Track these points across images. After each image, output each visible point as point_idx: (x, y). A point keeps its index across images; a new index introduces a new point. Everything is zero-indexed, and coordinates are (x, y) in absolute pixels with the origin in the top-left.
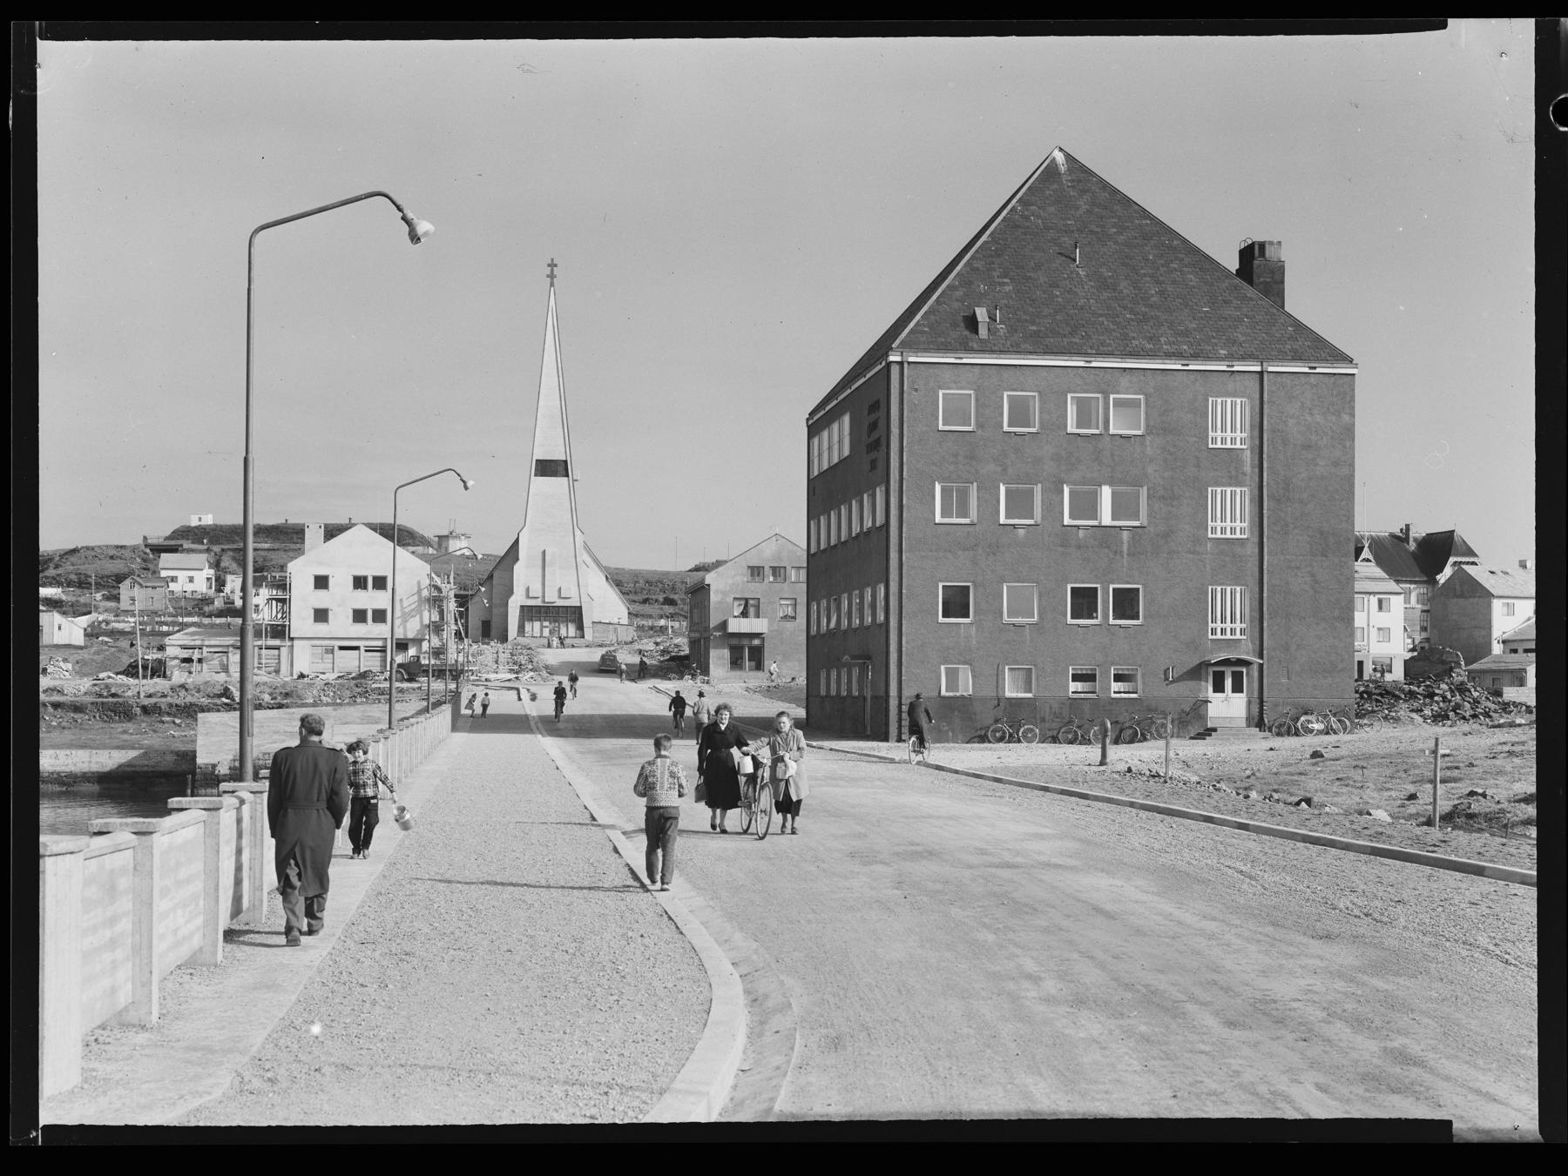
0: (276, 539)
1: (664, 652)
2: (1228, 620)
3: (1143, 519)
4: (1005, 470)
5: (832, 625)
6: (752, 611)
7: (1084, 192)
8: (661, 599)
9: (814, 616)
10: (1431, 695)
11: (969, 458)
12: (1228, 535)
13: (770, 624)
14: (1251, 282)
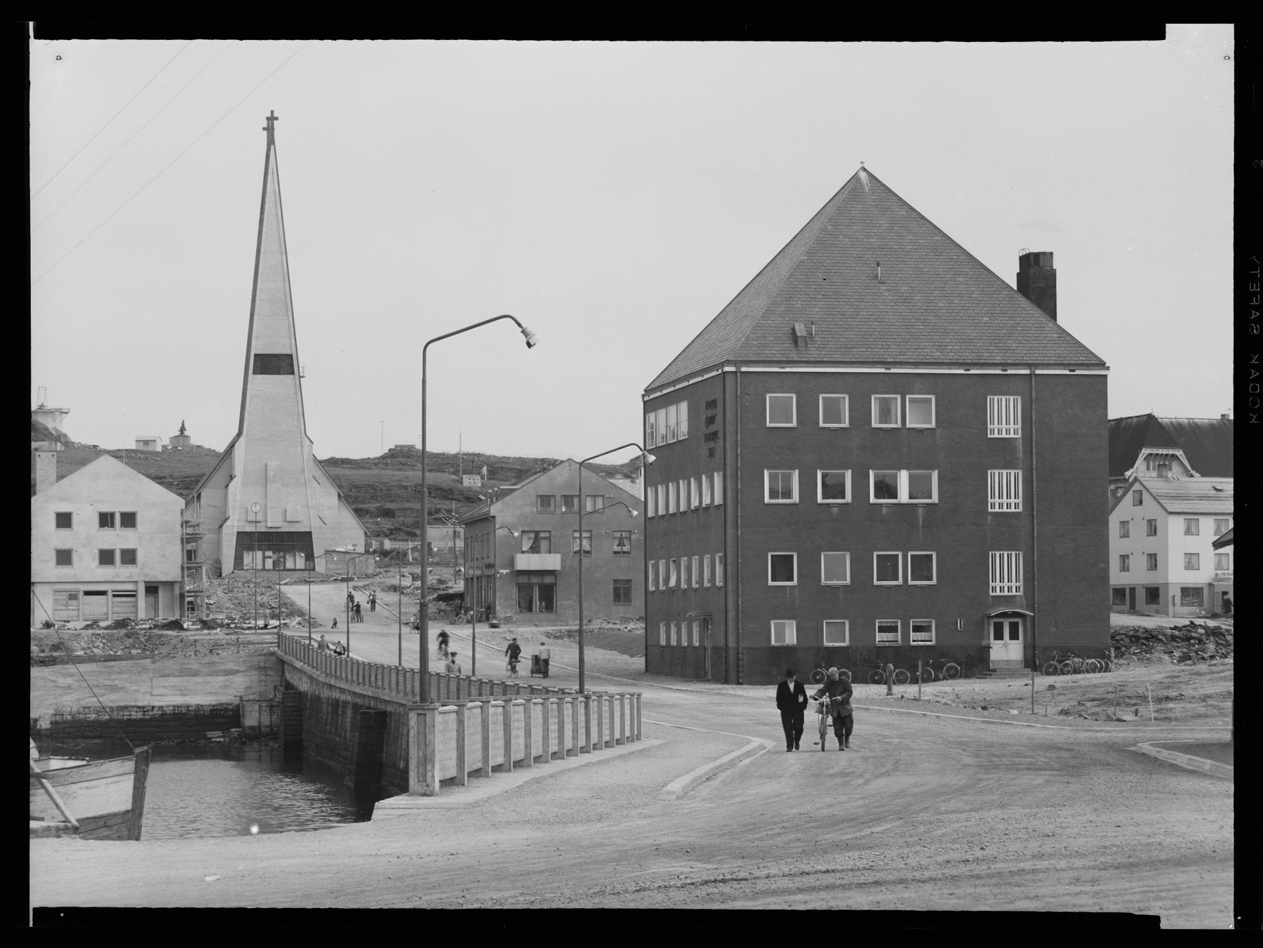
5: (672, 583)
6: (544, 545)
12: (1005, 510)
13: (563, 561)
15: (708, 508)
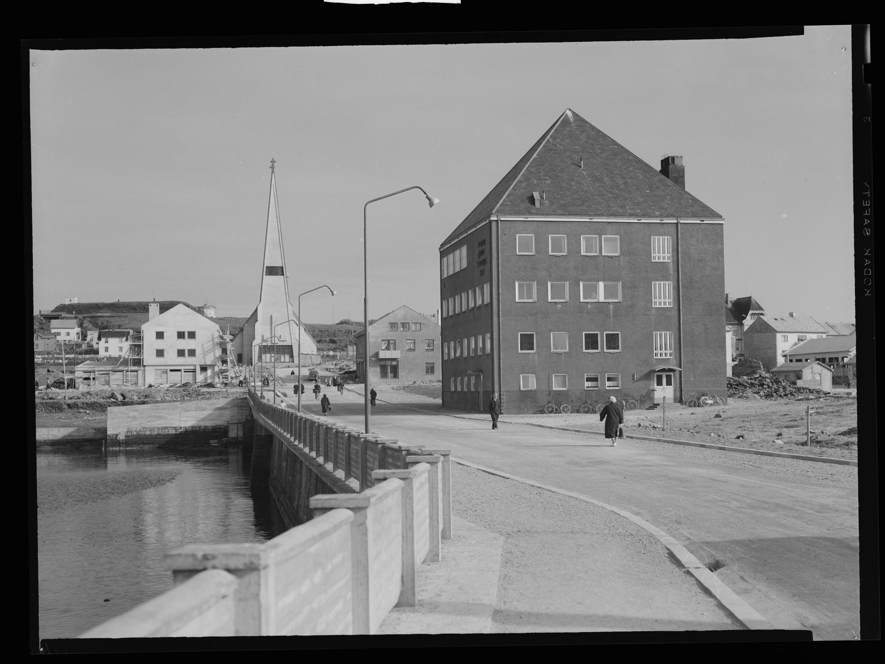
0: (113, 311)
1: (341, 369)
3: (620, 299)
4: (550, 274)
5: (458, 354)
6: (392, 346)
7: (583, 131)
8: (328, 340)
9: (446, 351)
10: (762, 385)
11: (535, 268)
13: (402, 353)
14: (668, 177)
15: (480, 307)
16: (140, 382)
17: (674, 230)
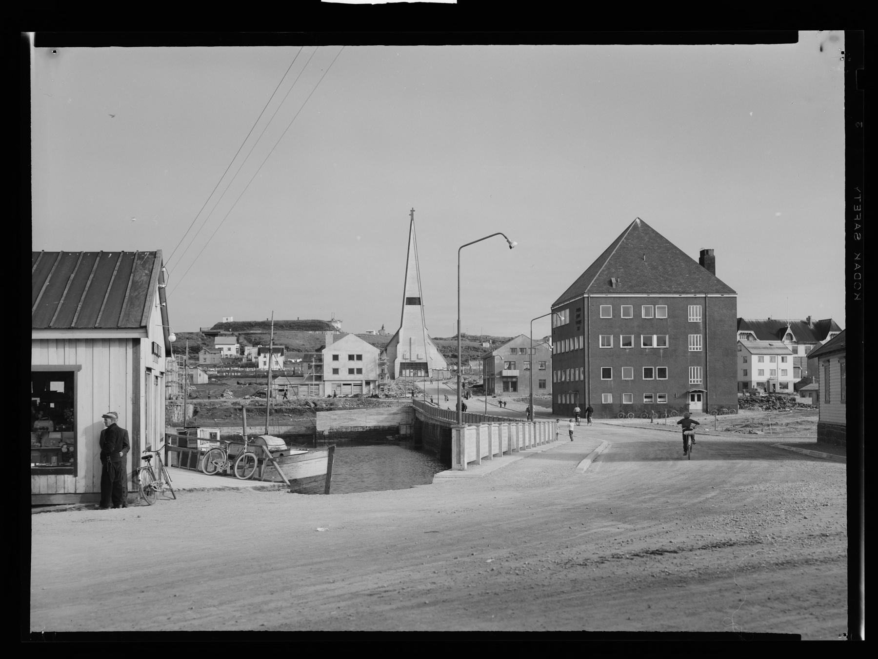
0: (264, 328)
2: (696, 378)
6: (512, 367)
8: (450, 354)
16: (321, 393)
17: (703, 301)
